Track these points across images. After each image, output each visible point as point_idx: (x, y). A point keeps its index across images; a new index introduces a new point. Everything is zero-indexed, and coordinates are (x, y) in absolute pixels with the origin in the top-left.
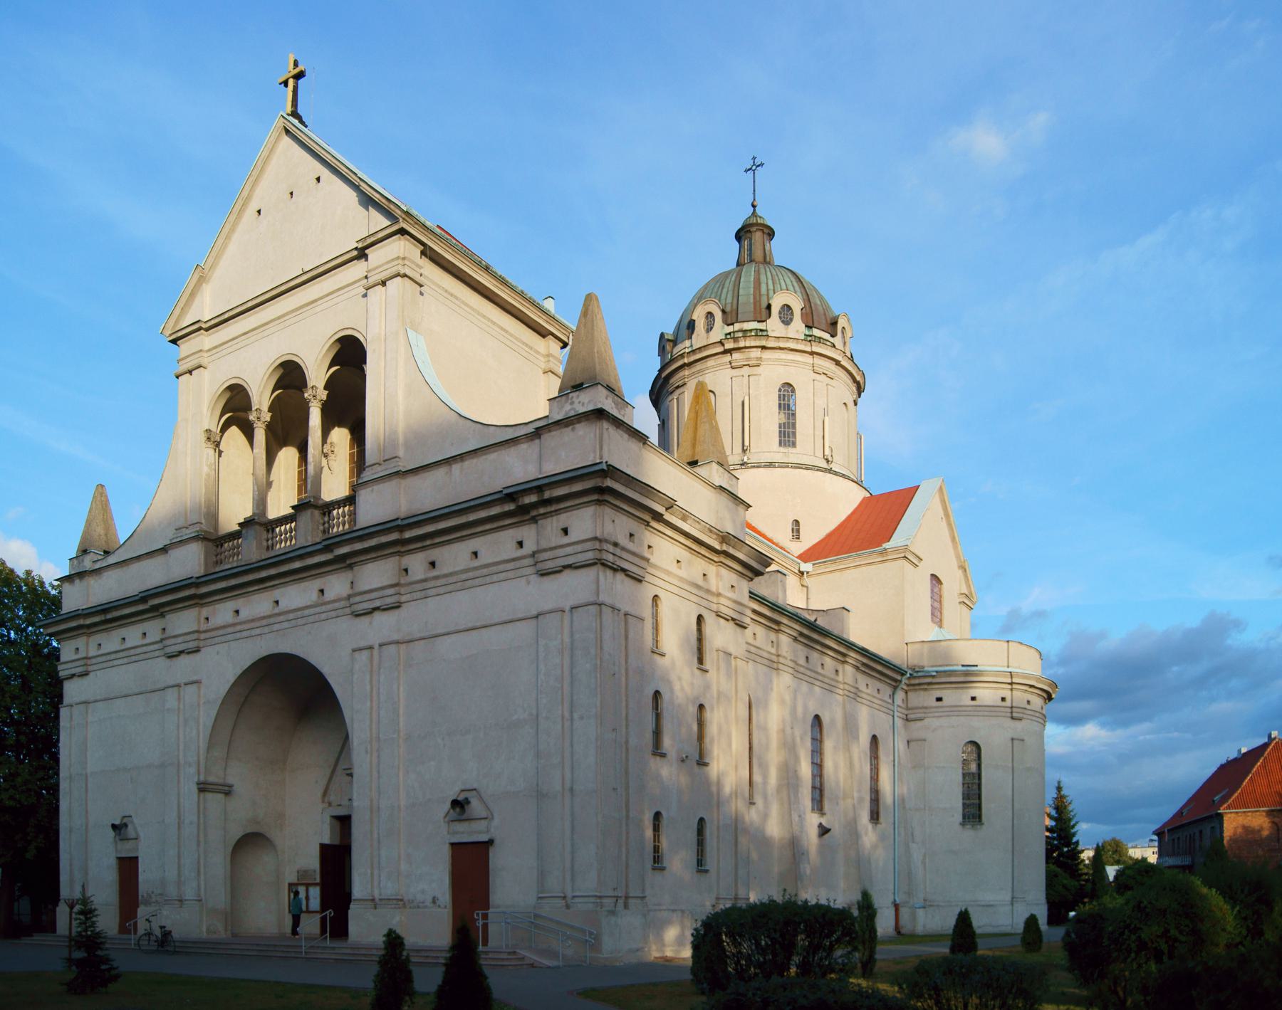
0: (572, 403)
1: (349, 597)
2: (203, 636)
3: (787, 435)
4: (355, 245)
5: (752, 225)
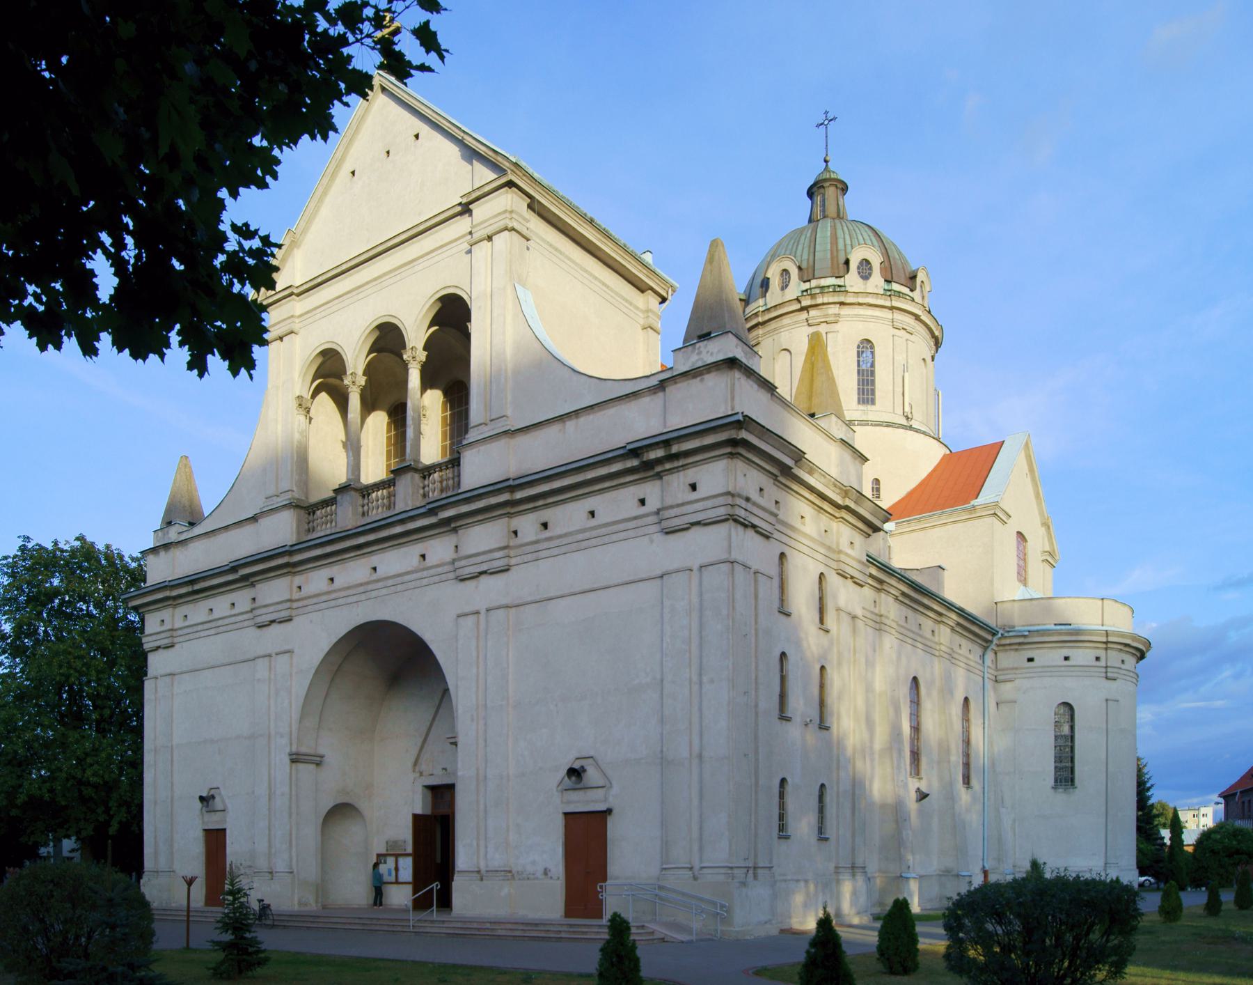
0: (699, 353)
1: (454, 561)
2: (295, 605)
3: (867, 392)
4: (460, 200)
5: (825, 180)
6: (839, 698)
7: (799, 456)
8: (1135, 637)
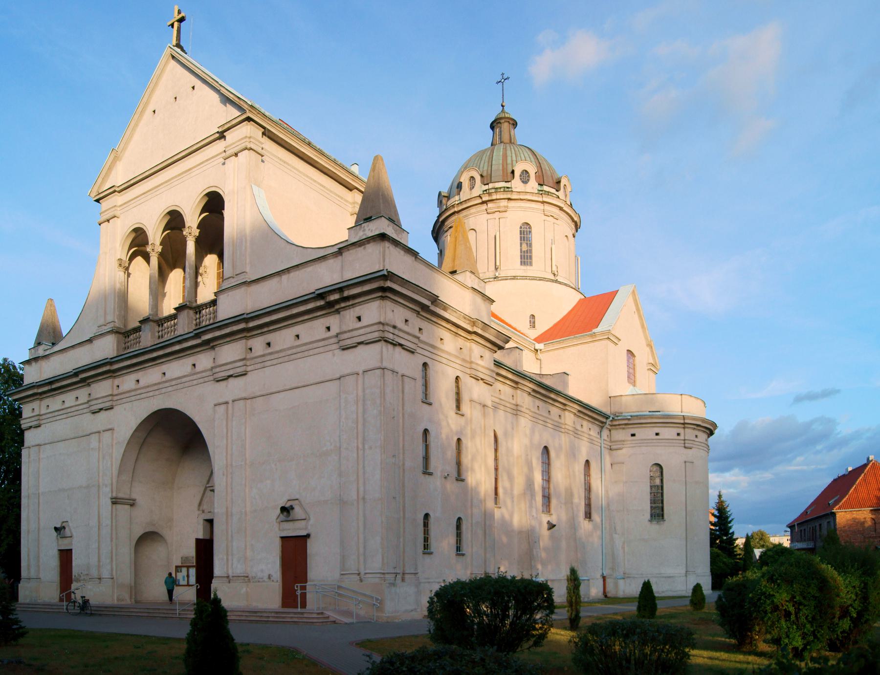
0: (364, 231)
1: (212, 368)
2: (115, 398)
3: (526, 258)
5: (501, 118)
6: (473, 459)
7: (435, 299)
8: (704, 420)
